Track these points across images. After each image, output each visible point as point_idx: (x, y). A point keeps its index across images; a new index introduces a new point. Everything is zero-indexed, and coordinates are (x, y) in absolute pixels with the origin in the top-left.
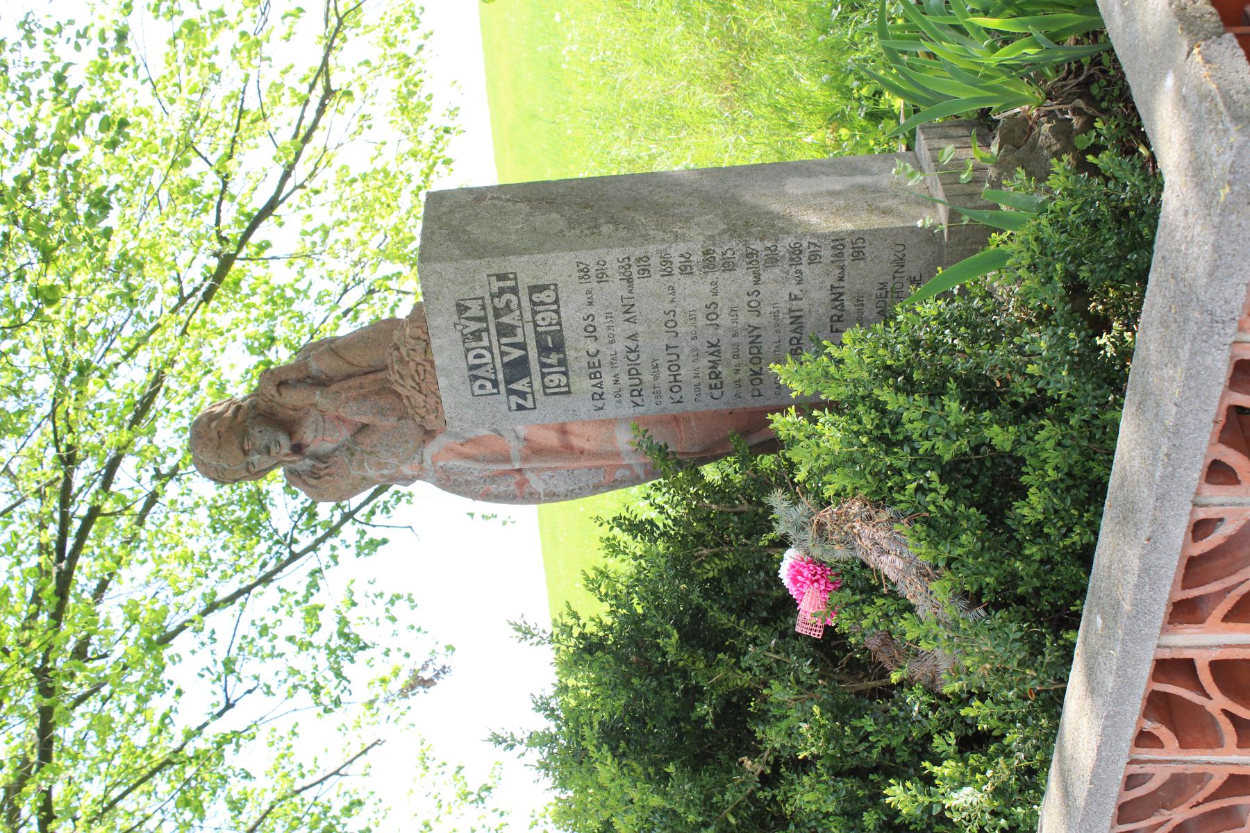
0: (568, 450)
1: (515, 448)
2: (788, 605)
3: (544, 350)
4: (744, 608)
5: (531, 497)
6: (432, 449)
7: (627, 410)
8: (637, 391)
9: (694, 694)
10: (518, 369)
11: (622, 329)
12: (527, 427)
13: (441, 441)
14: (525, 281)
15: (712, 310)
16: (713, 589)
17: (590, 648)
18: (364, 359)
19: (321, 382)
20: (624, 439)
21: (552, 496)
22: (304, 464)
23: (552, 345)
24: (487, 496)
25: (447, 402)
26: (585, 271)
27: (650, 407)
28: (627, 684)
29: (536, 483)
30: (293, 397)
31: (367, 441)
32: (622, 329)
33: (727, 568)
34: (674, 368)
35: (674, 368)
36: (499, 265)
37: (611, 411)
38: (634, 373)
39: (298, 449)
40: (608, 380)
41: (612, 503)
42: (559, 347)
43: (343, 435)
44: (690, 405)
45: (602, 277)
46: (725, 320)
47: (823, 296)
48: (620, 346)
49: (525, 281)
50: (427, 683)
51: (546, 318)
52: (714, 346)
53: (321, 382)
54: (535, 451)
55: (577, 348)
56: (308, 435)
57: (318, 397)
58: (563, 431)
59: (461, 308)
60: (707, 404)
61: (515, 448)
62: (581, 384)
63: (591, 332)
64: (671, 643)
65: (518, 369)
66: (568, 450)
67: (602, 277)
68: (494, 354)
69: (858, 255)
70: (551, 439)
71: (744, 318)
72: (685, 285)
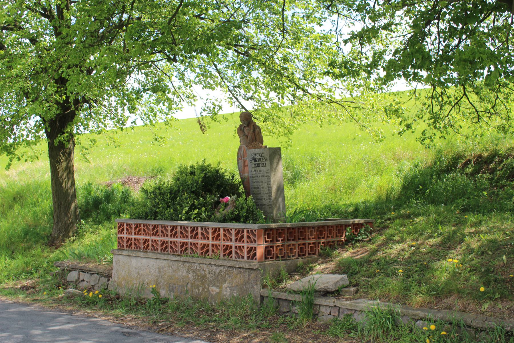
0: (245, 166)
1: (245, 158)
2: (223, 198)
3: (258, 164)
4: (222, 192)
5: (238, 160)
6: (245, 146)
7: (250, 176)
8: (252, 177)
9: (212, 186)
10: (255, 160)
11: (260, 175)
12: (248, 162)
13: (246, 148)
14: (266, 162)
15: (263, 188)
16: (225, 188)
17: (217, 171)
18: (257, 137)
19: (254, 131)
20: (246, 175)
21: (238, 163)
22: (242, 128)
23: (258, 166)
24: (238, 154)
25: (251, 150)
26: (268, 170)
27: (250, 179)
28: (213, 177)
29: (240, 161)
30: (252, 127)
31: (245, 138)
32: (260, 175)
33: (393, 80)
34: (256, 182)
35: (256, 182)
36: (268, 159)
37: (250, 173)
38: (255, 177)
39: (245, 127)
40: (254, 173)
41: (237, 172)
42: (258, 166)
43: (247, 134)
44: (251, 184)
45: (267, 173)
46: (262, 189)
47: (265, 203)
48: (258, 175)
49: (266, 162)
50: (201, 128)
51: (262, 165)
52: (258, 188)
53: (254, 131)
54: (245, 161)
55: (258, 169)
56: (247, 128)
57: (252, 131)
58: (247, 166)
59: (263, 153)
60: (251, 187)
61: (245, 158)
62: (253, 169)
63: (260, 171)
64: (218, 183)
65: (255, 160)
66: (245, 166)
67: (267, 173)
68: (258, 157)
69: (270, 208)
70: (246, 164)
71: (262, 192)
72: (266, 184)
